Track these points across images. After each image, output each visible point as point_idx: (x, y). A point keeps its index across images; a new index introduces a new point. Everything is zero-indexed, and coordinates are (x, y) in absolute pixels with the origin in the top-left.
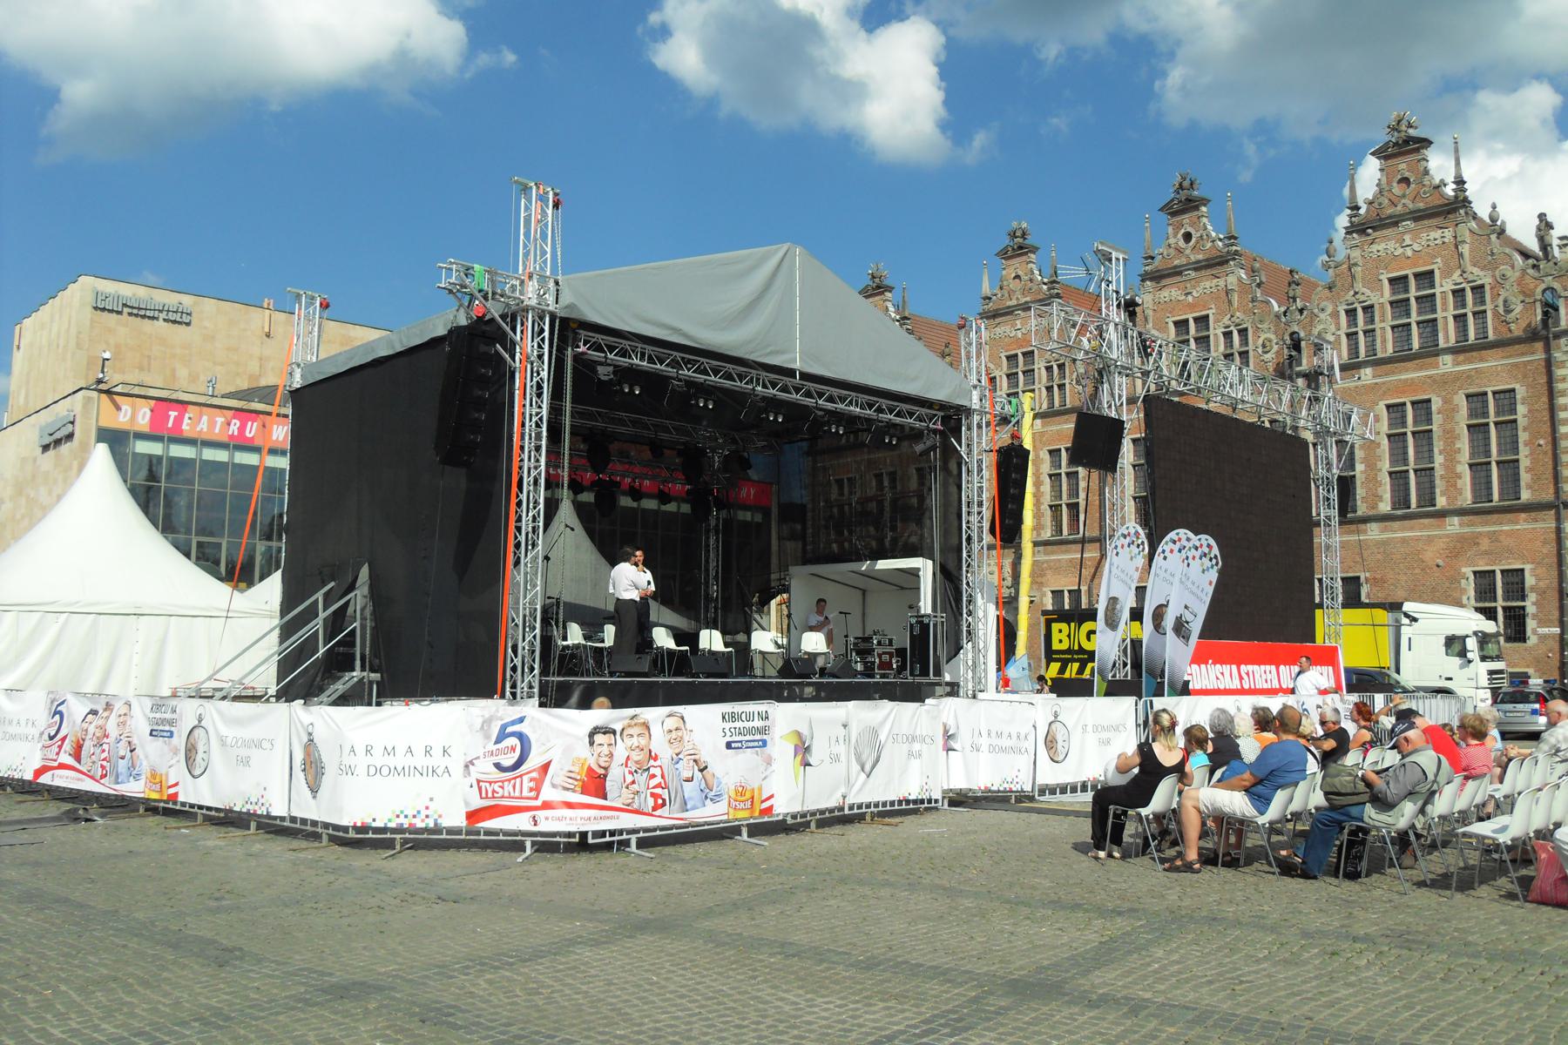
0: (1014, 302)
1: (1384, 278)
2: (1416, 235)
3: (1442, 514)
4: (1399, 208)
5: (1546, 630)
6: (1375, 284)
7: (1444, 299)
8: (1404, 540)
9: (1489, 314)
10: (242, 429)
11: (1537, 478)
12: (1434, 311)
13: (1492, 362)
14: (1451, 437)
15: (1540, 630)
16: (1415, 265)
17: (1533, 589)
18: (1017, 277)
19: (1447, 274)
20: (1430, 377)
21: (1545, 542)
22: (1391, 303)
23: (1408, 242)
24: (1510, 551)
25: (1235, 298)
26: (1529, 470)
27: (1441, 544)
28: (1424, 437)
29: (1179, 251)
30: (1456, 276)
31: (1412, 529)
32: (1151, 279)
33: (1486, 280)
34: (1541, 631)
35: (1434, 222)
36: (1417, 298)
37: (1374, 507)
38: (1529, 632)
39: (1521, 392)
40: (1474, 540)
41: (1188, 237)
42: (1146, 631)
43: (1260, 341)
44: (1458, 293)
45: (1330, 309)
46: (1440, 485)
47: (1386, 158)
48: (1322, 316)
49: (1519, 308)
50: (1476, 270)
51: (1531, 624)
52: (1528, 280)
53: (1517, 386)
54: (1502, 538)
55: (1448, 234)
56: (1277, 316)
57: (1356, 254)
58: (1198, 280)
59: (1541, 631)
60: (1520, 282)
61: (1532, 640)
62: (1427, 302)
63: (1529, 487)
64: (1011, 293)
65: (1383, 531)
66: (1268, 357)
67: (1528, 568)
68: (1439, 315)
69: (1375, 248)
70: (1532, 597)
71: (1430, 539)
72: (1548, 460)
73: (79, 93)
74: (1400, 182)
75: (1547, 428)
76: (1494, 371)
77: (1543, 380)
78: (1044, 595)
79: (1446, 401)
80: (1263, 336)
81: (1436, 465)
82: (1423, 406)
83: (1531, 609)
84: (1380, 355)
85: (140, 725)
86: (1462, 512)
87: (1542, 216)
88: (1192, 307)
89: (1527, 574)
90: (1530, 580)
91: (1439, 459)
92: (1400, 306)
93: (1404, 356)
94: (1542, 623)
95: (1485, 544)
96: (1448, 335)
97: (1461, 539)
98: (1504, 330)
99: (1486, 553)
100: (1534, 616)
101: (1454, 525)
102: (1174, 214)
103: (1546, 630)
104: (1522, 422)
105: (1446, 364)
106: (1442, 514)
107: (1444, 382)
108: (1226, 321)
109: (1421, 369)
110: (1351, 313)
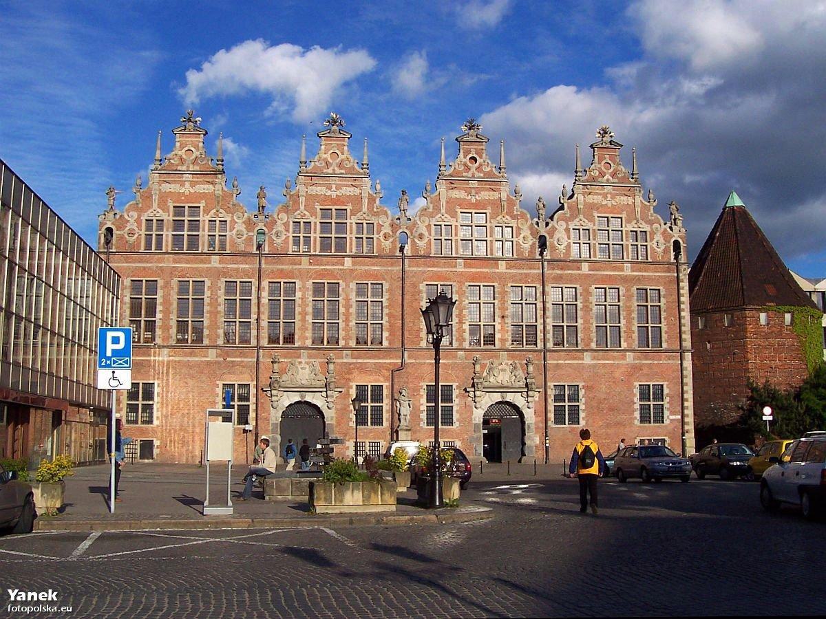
7: (351, 227)
10: (683, 264)
11: (669, 337)
17: (667, 395)
20: (619, 275)
26: (666, 333)
34: (671, 417)
51: (666, 413)
54: (654, 367)
59: (671, 417)
61: (667, 422)
67: (665, 384)
70: (667, 400)
73: (360, 46)
79: (628, 290)
83: (666, 405)
85: (783, 398)
89: (665, 387)
90: (666, 391)
94: (672, 413)
95: (645, 371)
96: (352, 248)
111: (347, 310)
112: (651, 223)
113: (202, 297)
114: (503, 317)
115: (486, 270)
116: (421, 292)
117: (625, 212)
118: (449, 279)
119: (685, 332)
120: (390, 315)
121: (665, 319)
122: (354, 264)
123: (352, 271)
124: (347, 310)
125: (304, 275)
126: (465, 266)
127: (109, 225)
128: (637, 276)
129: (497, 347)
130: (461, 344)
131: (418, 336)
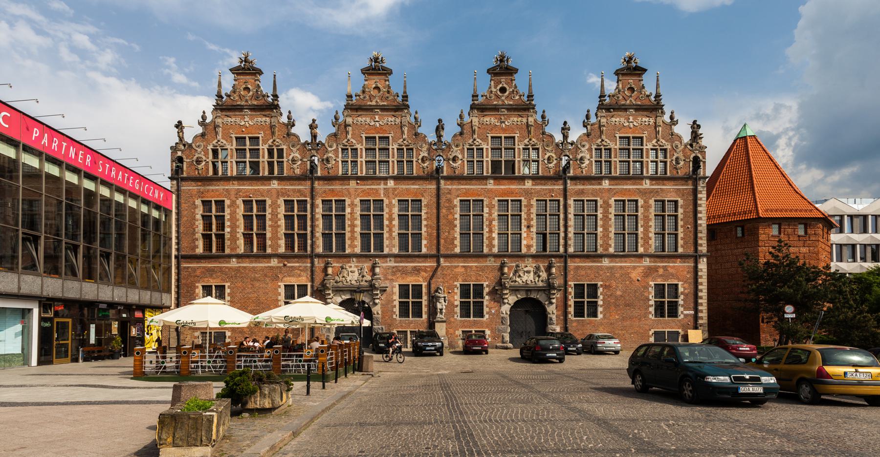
0: (374, 103)
1: (363, 136)
2: (381, 117)
3: (641, 256)
4: (628, 102)
5: (688, 312)
6: (485, 139)
8: (621, 267)
9: (414, 163)
11: (686, 243)
12: (258, 157)
13: (669, 186)
14: (647, 219)
15: (685, 312)
16: (634, 133)
17: (682, 293)
18: (377, 88)
19: (650, 140)
21: (688, 272)
22: (237, 150)
23: (377, 119)
24: (672, 275)
25: (406, 129)
27: (640, 270)
28: (262, 218)
29: (497, 97)
30: (526, 141)
31: (626, 262)
32: (478, 109)
33: (669, 147)
34: (685, 312)
35: (645, 113)
36: (250, 150)
37: (607, 250)
38: (485, 313)
39: (681, 202)
40: (656, 269)
41: (503, 90)
42: (865, 307)
43: (546, 157)
44: (270, 152)
45: (587, 147)
46: (227, 243)
47: (238, 74)
48: (583, 149)
49: (682, 163)
50: (664, 141)
51: (681, 309)
52: (687, 150)
53: (523, 199)
55: (652, 121)
56: (557, 145)
57: (219, 121)
58: (509, 116)
60: (683, 151)
62: (255, 152)
63: (682, 246)
64: (371, 98)
65: (611, 262)
66: (551, 165)
68: (261, 160)
69: (613, 119)
71: (634, 268)
72: (692, 235)
74: (629, 89)
75: (691, 220)
76: (670, 191)
77: (691, 198)
78: (393, 287)
79: (645, 202)
80: (548, 154)
81: (423, 232)
82: (262, 204)
83: (681, 302)
84: (613, 174)
86: (650, 256)
87: (440, 121)
88: (504, 130)
89: (680, 286)
90: (681, 289)
91: (641, 229)
92: (241, 152)
93: (626, 178)
95: (661, 271)
97: (649, 268)
98: (675, 172)
99: (661, 275)
100: (682, 306)
101: (647, 262)
102: (496, 74)
103: (688, 312)
104: (424, 216)
105: (647, 185)
106: (641, 256)
107: (644, 193)
108: (526, 141)
109: (634, 184)
110: (599, 150)
130: (490, 250)
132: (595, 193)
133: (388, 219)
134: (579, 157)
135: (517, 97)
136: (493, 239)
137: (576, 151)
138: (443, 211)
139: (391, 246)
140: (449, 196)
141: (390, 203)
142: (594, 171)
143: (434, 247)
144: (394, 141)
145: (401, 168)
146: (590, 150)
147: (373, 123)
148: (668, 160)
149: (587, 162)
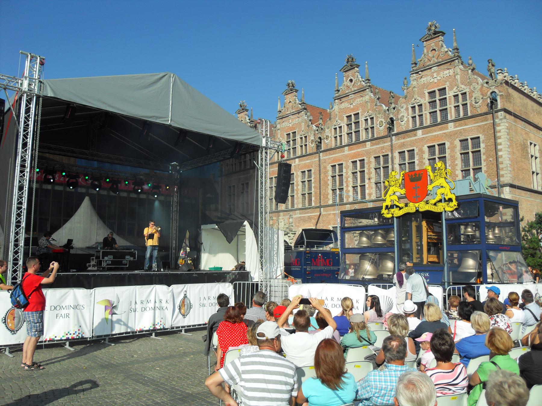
2: (438, 73)
9: (468, 105)
16: (438, 86)
23: (435, 76)
45: (405, 107)
48: (402, 110)
50: (463, 86)
52: (484, 89)
58: (355, 99)
60: (481, 90)
62: (443, 101)
79: (451, 143)
111: (347, 179)
112: (470, 84)
113: (478, 149)
114: (369, 179)
115: (359, 150)
116: (328, 171)
117: (448, 83)
118: (340, 160)
119: (502, 169)
120: (315, 187)
121: (484, 161)
122: (299, 161)
123: (299, 165)
124: (297, 188)
125: (368, 153)
126: (349, 150)
127: (391, 116)
128: (458, 130)
129: (367, 199)
130: (348, 200)
131: (327, 198)
132: (412, 143)
133: (367, 174)
134: (399, 117)
135: (359, 83)
136: (349, 191)
137: (398, 112)
138: (322, 175)
139: (298, 203)
140: (325, 164)
141: (297, 174)
142: (411, 127)
143: (318, 202)
144: (298, 133)
145: (458, 111)
146: (407, 109)
147: (432, 80)
148: (468, 102)
149: (405, 119)
